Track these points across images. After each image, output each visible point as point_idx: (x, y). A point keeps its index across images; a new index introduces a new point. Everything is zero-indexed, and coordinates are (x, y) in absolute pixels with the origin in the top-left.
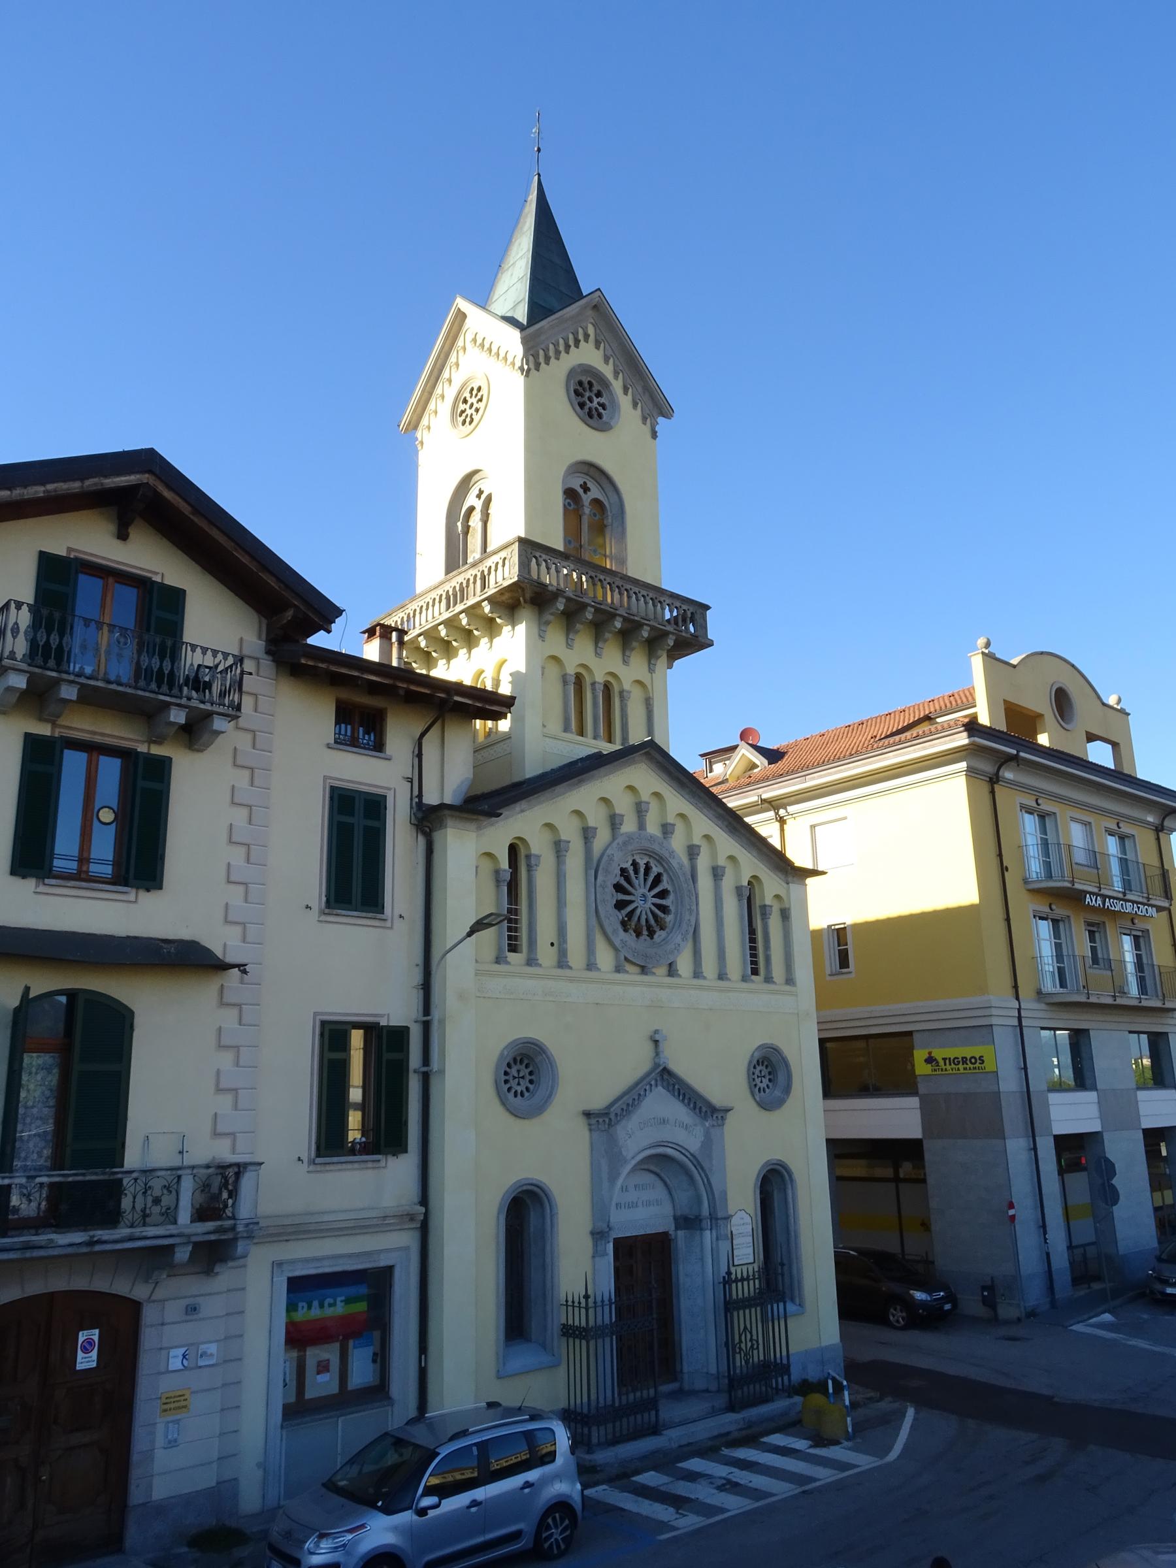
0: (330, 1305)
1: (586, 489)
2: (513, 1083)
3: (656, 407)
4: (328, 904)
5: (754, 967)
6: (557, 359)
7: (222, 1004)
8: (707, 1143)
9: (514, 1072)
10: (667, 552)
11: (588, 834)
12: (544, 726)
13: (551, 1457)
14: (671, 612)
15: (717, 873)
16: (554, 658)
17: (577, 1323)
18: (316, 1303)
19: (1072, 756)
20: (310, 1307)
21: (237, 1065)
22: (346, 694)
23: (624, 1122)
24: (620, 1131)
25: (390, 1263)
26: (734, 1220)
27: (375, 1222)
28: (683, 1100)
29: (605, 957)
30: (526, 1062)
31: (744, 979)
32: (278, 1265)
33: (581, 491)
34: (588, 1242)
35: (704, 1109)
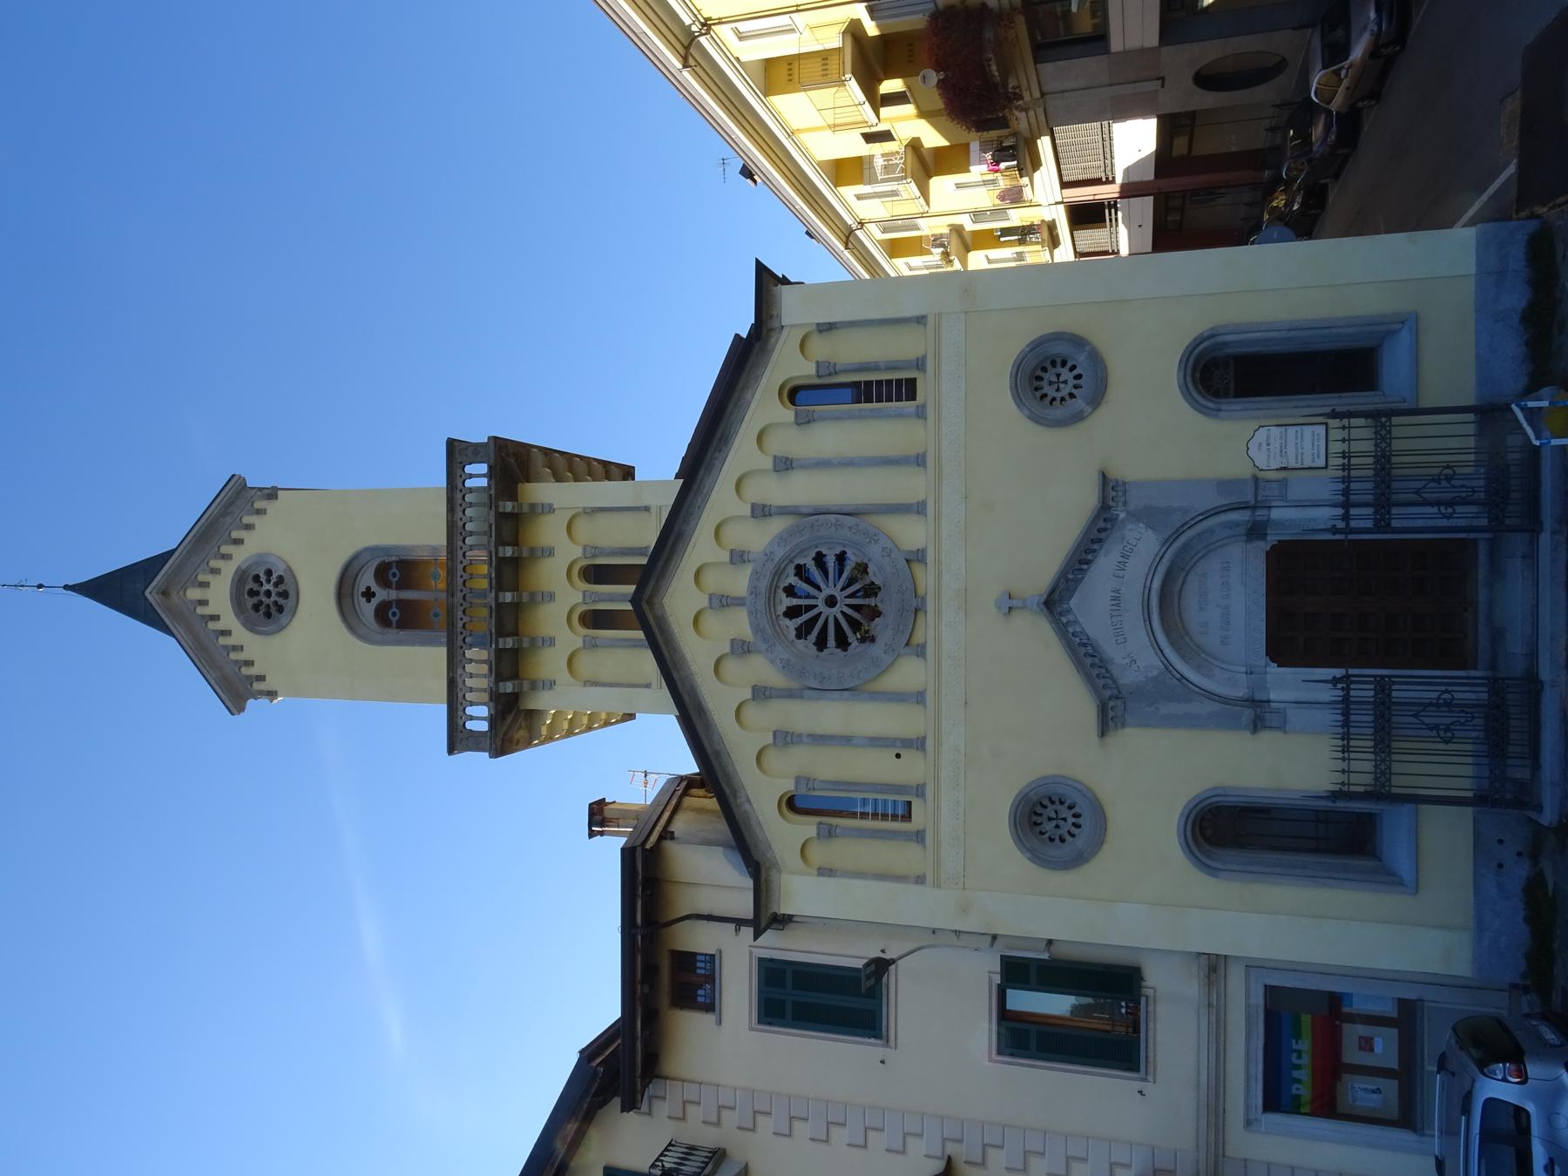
0: (1299, 1057)
1: (369, 595)
2: (1063, 831)
3: (237, 502)
4: (878, 1036)
5: (906, 390)
7: (983, 1164)
8: (1148, 516)
9: (1049, 827)
10: (400, 493)
11: (761, 693)
13: (1519, 1113)
15: (784, 465)
18: (1296, 1074)
20: (1299, 1081)
21: (1043, 1154)
22: (664, 999)
23: (1116, 673)
25: (1261, 991)
26: (1261, 463)
27: (1213, 1018)
28: (1088, 562)
29: (907, 674)
31: (921, 414)
32: (1248, 1123)
33: (375, 601)
34: (1266, 736)
35: (1102, 525)
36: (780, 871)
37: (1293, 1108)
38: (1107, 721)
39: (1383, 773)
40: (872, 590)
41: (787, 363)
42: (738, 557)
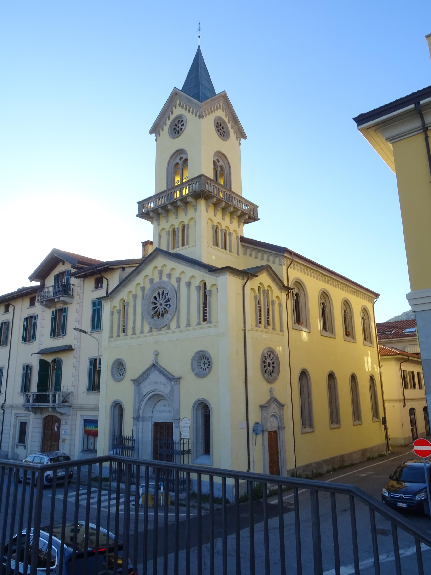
1: (218, 161)
3: (241, 134)
6: (209, 115)
7: (74, 357)
11: (143, 289)
12: (207, 243)
14: (247, 207)
15: (189, 284)
16: (210, 219)
17: (182, 449)
19: (259, 242)
23: (143, 383)
24: (142, 386)
26: (183, 421)
30: (202, 358)
32: (81, 416)
33: (217, 162)
36: (111, 301)
37: (85, 426)
38: (134, 381)
39: (184, 453)
40: (163, 315)
41: (210, 279)
42: (169, 276)
